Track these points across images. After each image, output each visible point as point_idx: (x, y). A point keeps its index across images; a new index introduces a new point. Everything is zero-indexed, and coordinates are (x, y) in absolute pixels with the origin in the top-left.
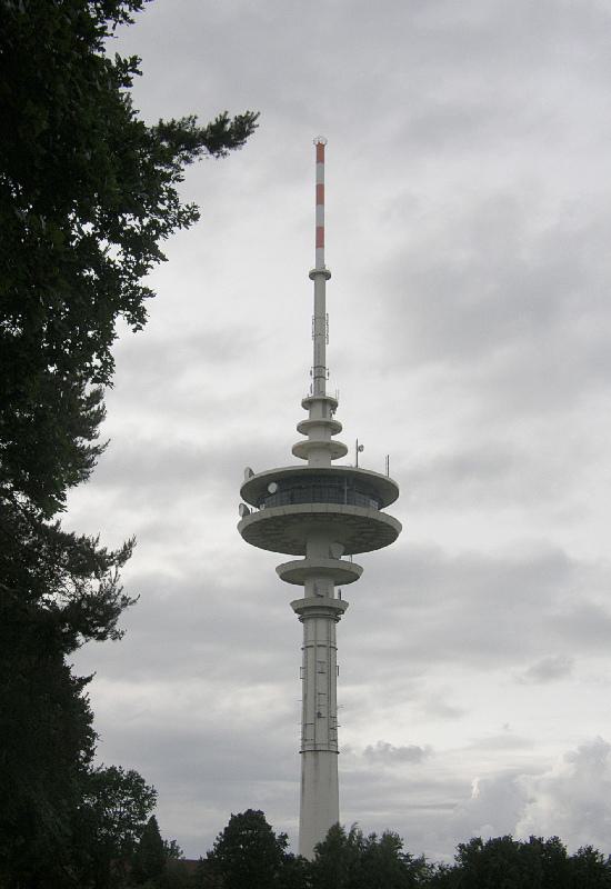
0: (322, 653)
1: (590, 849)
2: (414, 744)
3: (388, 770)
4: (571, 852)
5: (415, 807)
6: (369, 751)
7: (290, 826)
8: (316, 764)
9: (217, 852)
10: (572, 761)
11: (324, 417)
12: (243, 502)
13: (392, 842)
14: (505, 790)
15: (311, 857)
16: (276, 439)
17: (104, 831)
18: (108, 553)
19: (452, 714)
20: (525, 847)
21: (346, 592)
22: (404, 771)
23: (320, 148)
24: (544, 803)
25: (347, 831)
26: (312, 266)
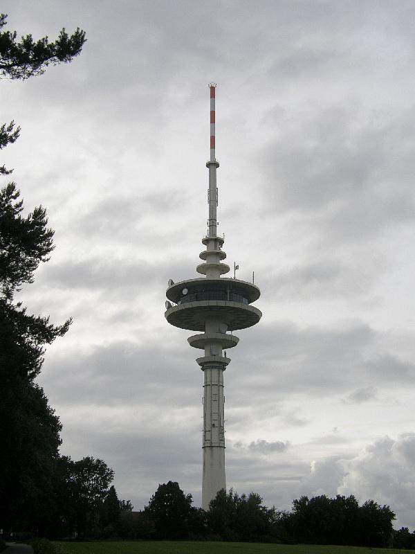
0: (215, 389)
1: (372, 502)
2: (280, 441)
3: (263, 457)
4: (361, 504)
5: (278, 479)
6: (252, 445)
7: (197, 493)
8: (212, 456)
9: (151, 507)
10: (370, 451)
11: (215, 248)
12: (168, 300)
13: (255, 499)
14: (331, 468)
15: (207, 509)
16: (186, 258)
17: (83, 495)
18: (54, 328)
19: (300, 423)
20: (333, 502)
21: (229, 353)
22: (272, 458)
23: (213, 89)
24: (354, 475)
25: (228, 493)
26: (208, 159)
